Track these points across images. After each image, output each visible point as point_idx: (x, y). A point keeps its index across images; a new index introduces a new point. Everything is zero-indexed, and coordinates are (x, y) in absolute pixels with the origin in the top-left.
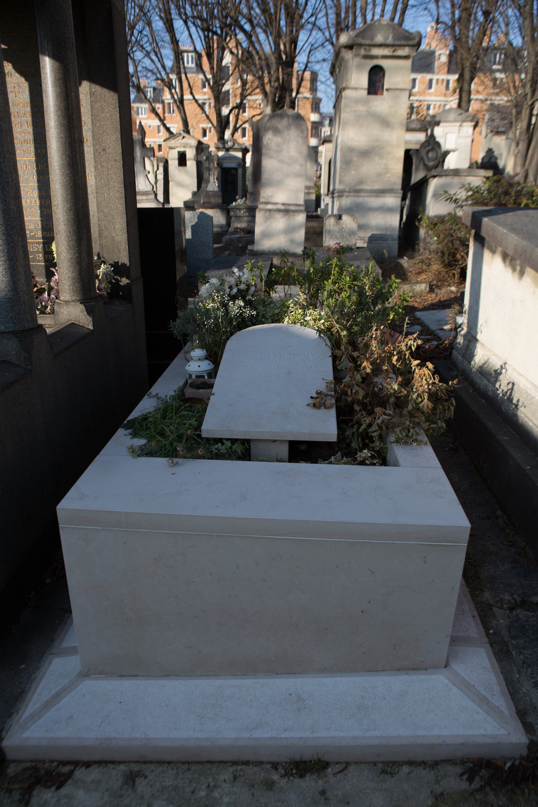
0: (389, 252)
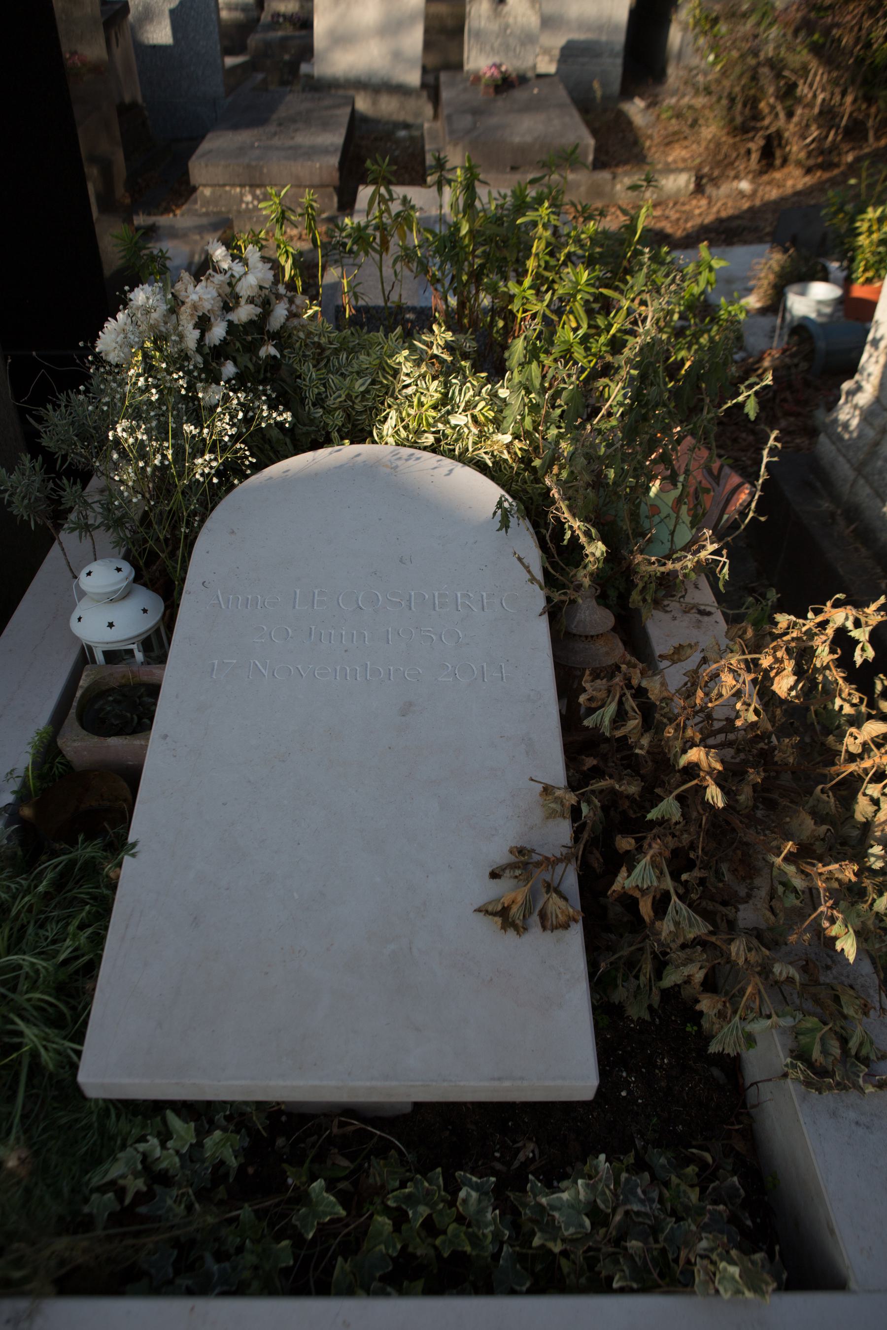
0: (603, 85)
